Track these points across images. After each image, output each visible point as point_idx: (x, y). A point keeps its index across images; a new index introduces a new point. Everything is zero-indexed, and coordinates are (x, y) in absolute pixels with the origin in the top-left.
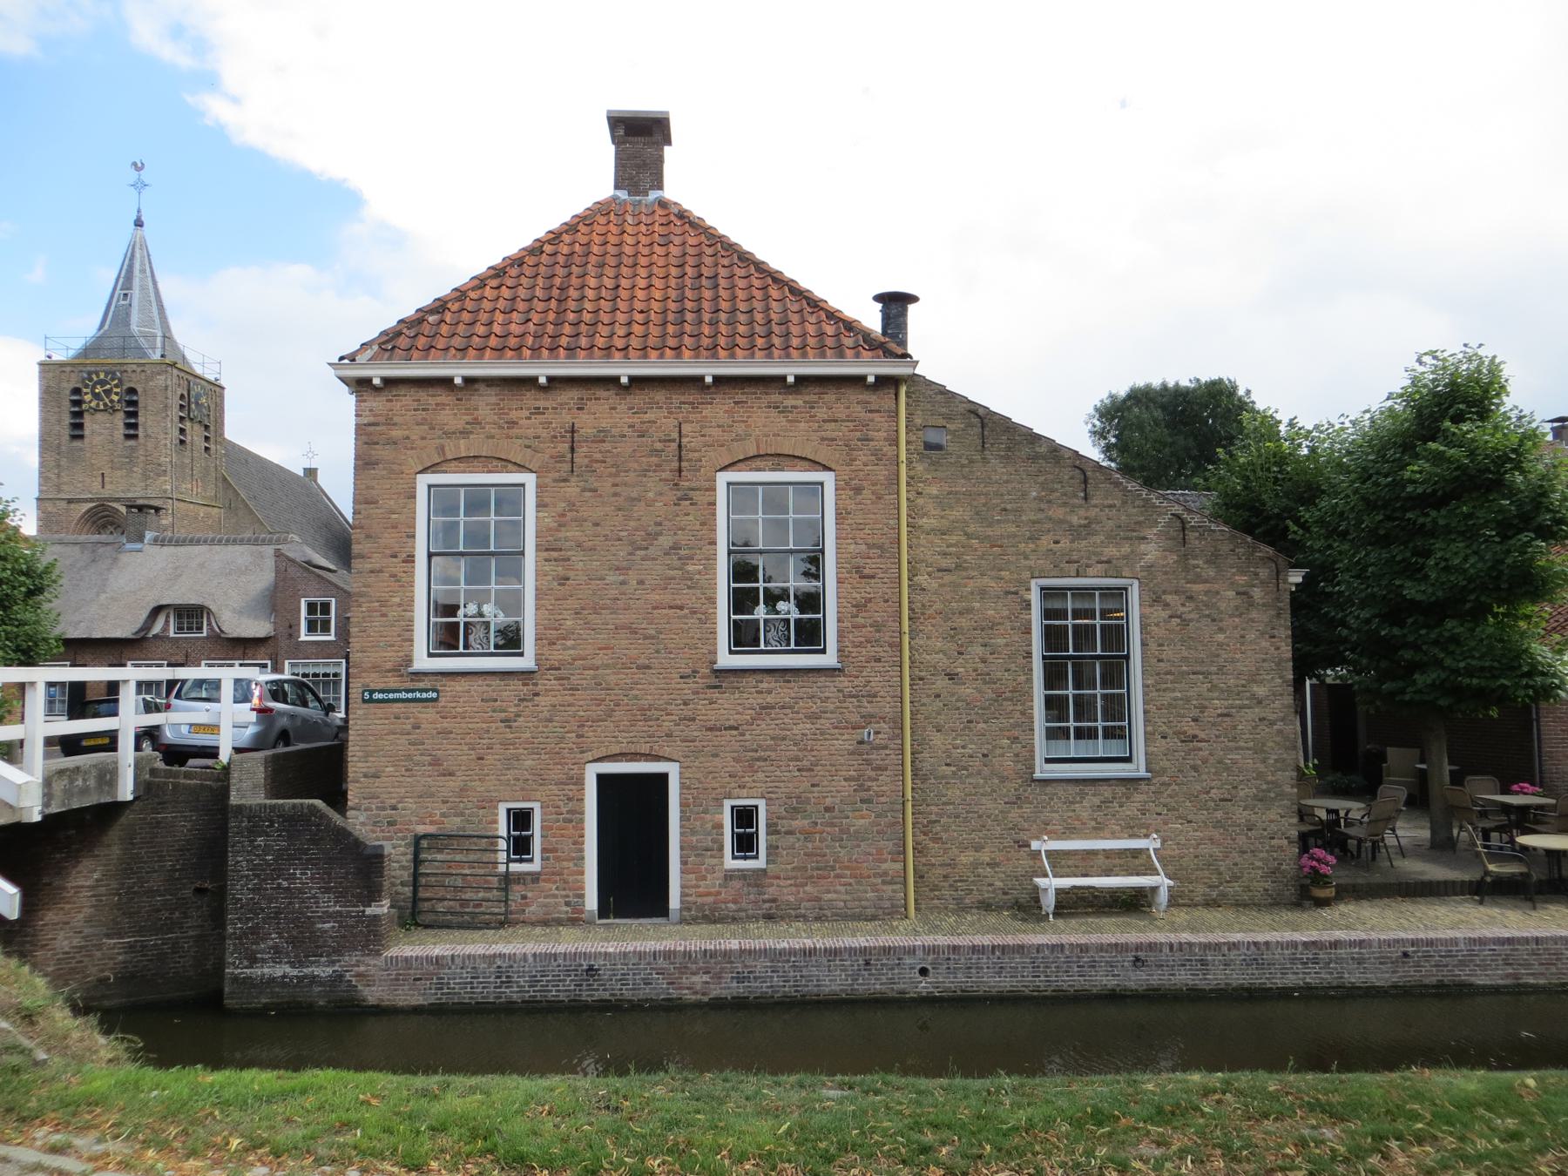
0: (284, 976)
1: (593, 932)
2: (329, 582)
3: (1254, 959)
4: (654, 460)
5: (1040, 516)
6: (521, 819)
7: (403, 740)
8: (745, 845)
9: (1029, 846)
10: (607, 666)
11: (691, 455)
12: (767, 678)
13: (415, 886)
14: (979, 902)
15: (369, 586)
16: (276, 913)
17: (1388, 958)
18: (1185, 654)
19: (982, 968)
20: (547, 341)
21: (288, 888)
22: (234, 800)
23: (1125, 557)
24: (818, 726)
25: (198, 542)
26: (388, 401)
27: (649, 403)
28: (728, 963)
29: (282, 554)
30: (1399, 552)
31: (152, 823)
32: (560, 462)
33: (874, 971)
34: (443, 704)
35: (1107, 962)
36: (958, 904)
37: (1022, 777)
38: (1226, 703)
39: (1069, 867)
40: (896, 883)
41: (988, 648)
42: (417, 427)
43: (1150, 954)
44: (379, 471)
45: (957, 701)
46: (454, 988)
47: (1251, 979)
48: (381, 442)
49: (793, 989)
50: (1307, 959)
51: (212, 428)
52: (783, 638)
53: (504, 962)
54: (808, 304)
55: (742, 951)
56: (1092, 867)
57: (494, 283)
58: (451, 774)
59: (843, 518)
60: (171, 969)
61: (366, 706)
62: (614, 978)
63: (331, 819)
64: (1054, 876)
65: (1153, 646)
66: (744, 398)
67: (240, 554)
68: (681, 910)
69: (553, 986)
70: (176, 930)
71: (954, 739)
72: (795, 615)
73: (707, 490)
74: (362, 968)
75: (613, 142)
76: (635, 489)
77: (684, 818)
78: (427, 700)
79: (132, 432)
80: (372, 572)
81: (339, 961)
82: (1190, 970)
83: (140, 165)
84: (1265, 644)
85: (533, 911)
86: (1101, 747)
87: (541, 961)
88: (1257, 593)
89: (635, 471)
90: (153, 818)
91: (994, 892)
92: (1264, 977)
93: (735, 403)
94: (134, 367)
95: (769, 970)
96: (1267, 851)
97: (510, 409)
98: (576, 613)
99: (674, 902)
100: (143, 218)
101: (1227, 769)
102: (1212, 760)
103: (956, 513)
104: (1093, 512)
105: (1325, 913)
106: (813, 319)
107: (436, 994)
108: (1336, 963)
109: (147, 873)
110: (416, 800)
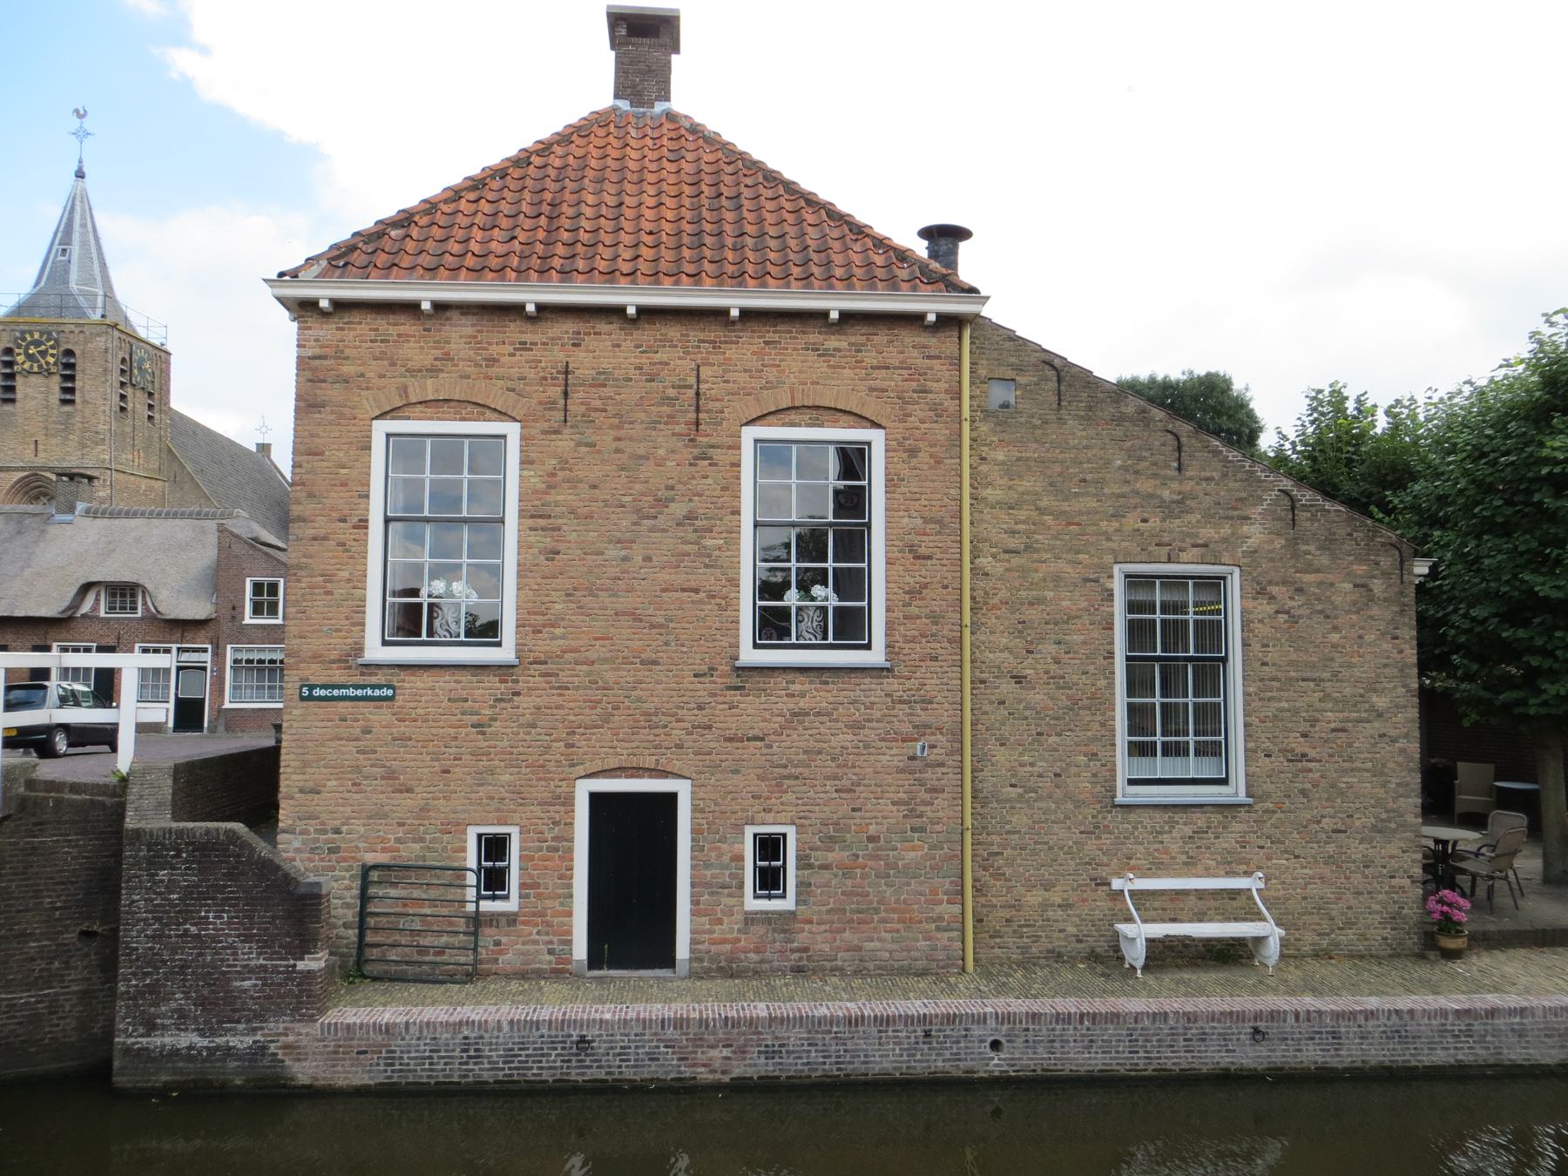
0: (190, 1048)
1: (582, 989)
2: (278, 561)
3: (1397, 1031)
4: (666, 409)
5: (1126, 489)
6: (495, 847)
7: (351, 747)
8: (770, 881)
9: (1109, 884)
10: (605, 661)
11: (711, 405)
12: (801, 678)
13: (362, 928)
14: (1049, 951)
15: (310, 557)
16: (182, 967)
17: (1555, 1029)
18: (1294, 657)
19: (1068, 1041)
20: (535, 262)
21: (198, 936)
22: (130, 822)
23: (1225, 540)
24: (861, 737)
25: (135, 515)
26: (338, 329)
27: (661, 341)
28: (755, 1033)
29: (227, 530)
30: (1524, 541)
31: (26, 849)
32: (549, 409)
33: (935, 1045)
34: (400, 703)
35: (1219, 1034)
36: (1022, 953)
37: (1101, 802)
38: (1341, 715)
39: (1155, 909)
40: (951, 930)
41: (1062, 646)
42: (374, 363)
43: (1270, 1024)
44: (325, 415)
45: (1026, 708)
46: (408, 1064)
47: (1393, 1055)
48: (330, 380)
49: (835, 1067)
50: (1460, 1031)
51: (156, 396)
52: (818, 630)
53: (473, 1031)
54: (851, 230)
55: (772, 1020)
56: (1183, 909)
57: (472, 196)
58: (410, 790)
59: (895, 486)
60: (46, 1033)
61: (305, 704)
62: (611, 1052)
63: (254, 849)
64: (1145, 921)
65: (1256, 647)
66: (776, 337)
67: (181, 529)
68: (691, 960)
69: (534, 1062)
70: (55, 984)
71: (1021, 754)
72: (833, 602)
73: (729, 448)
74: (291, 1038)
75: (613, 47)
76: (641, 445)
77: (696, 848)
78: (380, 699)
79: (68, 397)
80: (315, 539)
81: (262, 1028)
82: (1319, 1044)
83: (82, 112)
84: (1386, 646)
85: (509, 960)
86: (1192, 766)
87: (519, 1030)
88: (1378, 586)
89: (642, 422)
90: (29, 843)
91: (1065, 939)
92: (1407, 1052)
93: (766, 343)
94: (72, 327)
95: (806, 1043)
96: (1386, 893)
97: (490, 344)
98: (567, 595)
99: (682, 950)
100: (85, 170)
101: (1341, 794)
102: (1324, 784)
103: (1026, 484)
104: (1188, 486)
105: (1458, 967)
106: (857, 247)
107: (386, 1071)
108: (1493, 1036)
109: (19, 911)
110: (365, 821)
